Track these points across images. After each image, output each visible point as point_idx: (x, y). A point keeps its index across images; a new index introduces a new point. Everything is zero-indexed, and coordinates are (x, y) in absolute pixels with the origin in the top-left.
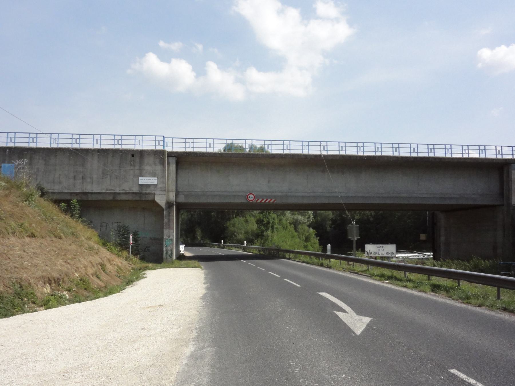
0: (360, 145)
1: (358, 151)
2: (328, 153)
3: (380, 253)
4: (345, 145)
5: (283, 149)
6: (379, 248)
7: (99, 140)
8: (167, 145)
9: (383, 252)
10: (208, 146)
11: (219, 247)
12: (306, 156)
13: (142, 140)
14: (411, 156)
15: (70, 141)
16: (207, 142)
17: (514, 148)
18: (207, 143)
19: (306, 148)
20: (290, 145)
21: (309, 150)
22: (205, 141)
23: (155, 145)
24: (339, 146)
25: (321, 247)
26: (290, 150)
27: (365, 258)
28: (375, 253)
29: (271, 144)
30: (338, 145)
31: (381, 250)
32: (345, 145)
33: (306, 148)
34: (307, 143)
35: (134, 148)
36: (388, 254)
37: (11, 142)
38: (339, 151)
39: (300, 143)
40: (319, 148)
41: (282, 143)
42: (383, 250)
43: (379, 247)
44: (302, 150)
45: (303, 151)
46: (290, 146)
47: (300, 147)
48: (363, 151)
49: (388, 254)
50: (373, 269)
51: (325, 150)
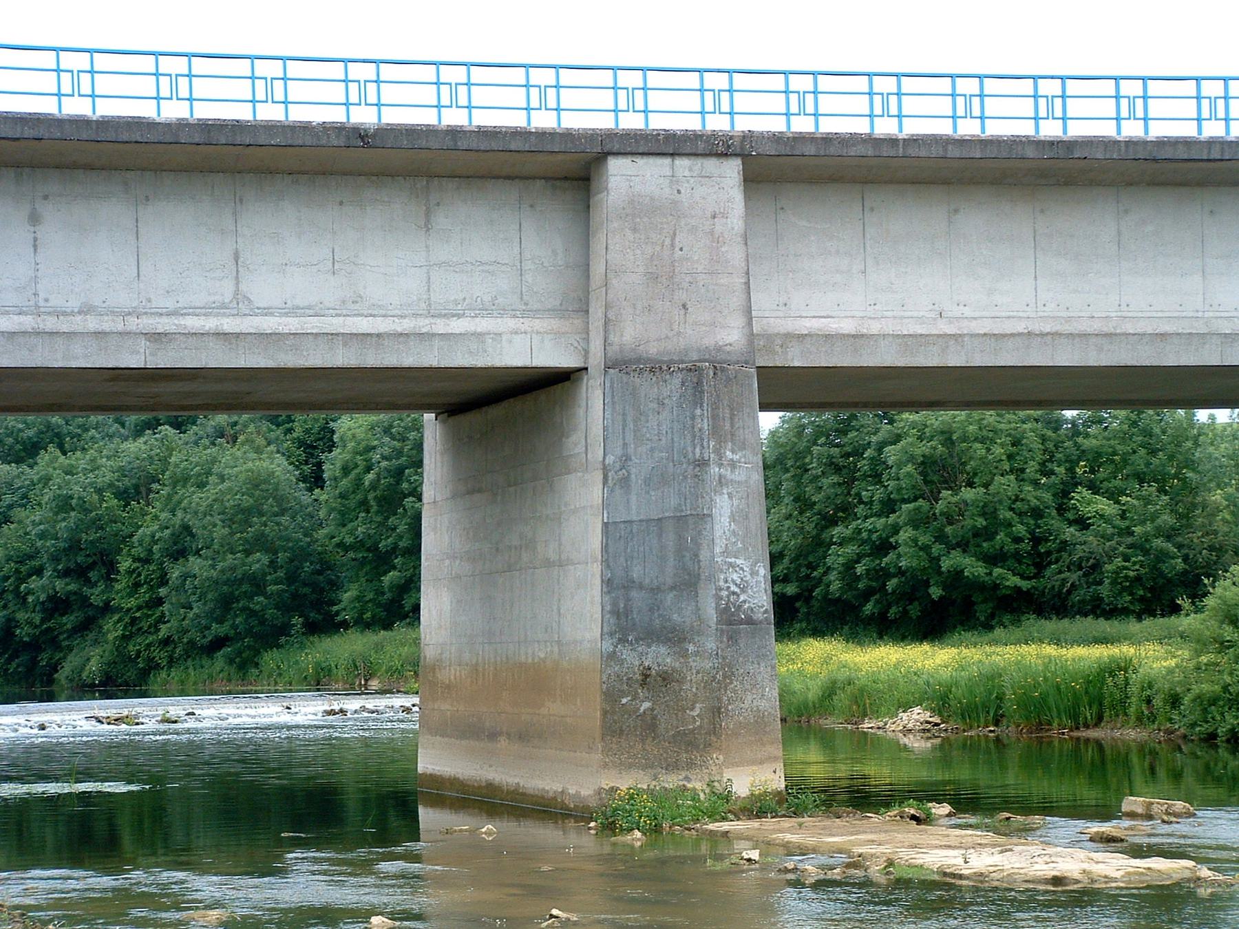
0: (1050, 88)
2: (258, 118)
4: (1064, 90)
7: (66, 88)
10: (260, 95)
12: (359, 137)
14: (158, 120)
15: (242, 89)
16: (257, 74)
17: (1236, 88)
18: (346, 81)
20: (557, 87)
21: (899, 116)
23: (158, 98)
24: (953, 95)
25: (484, 780)
26: (899, 116)
27: (1131, 828)
29: (557, 87)
30: (1195, 95)
32: (1064, 90)
35: (555, 125)
38: (954, 117)
41: (778, 82)
45: (959, 120)
46: (646, 96)
47: (862, 104)
48: (1145, 119)
51: (1138, 116)
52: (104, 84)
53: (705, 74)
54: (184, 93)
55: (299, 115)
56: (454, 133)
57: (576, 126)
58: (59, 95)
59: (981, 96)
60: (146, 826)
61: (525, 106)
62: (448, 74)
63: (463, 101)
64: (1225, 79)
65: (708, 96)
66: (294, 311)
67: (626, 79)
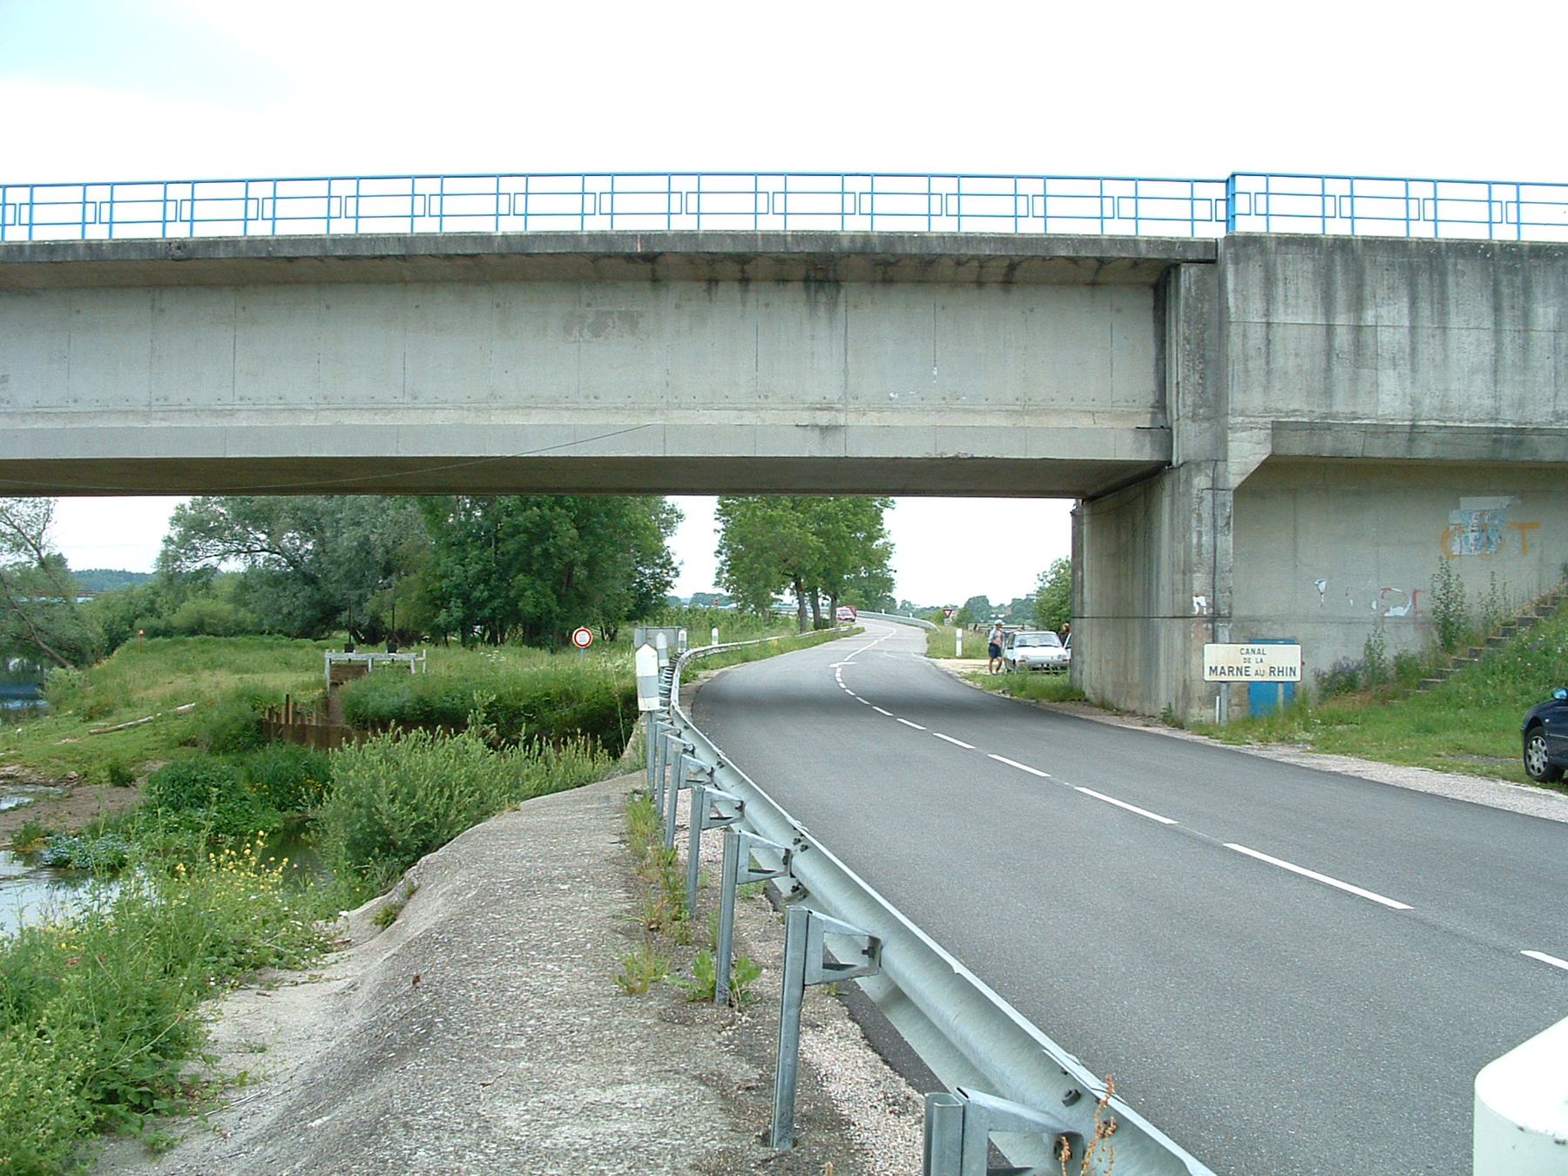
1: (87, 220)
3: (1252, 672)
5: (1407, 220)
6: (1247, 656)
7: (866, 199)
8: (1213, 210)
9: (1261, 667)
11: (196, 694)
13: (1267, 193)
19: (97, 213)
20: (1352, 196)
22: (835, 183)
24: (1490, 201)
28: (1235, 672)
31: (1253, 661)
33: (97, 213)
34: (1425, 190)
36: (1276, 672)
37: (1504, 221)
39: (1398, 189)
40: (1481, 212)
42: (1261, 661)
43: (1248, 653)
44: (1407, 220)
47: (1481, 212)
49: (1276, 672)
50: (179, 809)
52: (621, 203)
53: (1326, 180)
54: (779, 208)
55: (971, 227)
56: (93, 247)
57: (1174, 235)
58: (1102, 218)
59: (31, 204)
60: (907, 974)
61: (1405, 217)
62: (939, 185)
63: (1346, 212)
64: (1489, 183)
65: (1329, 201)
66: (1178, 433)
67: (1334, 187)
